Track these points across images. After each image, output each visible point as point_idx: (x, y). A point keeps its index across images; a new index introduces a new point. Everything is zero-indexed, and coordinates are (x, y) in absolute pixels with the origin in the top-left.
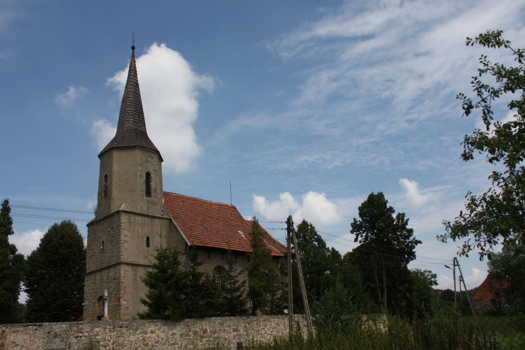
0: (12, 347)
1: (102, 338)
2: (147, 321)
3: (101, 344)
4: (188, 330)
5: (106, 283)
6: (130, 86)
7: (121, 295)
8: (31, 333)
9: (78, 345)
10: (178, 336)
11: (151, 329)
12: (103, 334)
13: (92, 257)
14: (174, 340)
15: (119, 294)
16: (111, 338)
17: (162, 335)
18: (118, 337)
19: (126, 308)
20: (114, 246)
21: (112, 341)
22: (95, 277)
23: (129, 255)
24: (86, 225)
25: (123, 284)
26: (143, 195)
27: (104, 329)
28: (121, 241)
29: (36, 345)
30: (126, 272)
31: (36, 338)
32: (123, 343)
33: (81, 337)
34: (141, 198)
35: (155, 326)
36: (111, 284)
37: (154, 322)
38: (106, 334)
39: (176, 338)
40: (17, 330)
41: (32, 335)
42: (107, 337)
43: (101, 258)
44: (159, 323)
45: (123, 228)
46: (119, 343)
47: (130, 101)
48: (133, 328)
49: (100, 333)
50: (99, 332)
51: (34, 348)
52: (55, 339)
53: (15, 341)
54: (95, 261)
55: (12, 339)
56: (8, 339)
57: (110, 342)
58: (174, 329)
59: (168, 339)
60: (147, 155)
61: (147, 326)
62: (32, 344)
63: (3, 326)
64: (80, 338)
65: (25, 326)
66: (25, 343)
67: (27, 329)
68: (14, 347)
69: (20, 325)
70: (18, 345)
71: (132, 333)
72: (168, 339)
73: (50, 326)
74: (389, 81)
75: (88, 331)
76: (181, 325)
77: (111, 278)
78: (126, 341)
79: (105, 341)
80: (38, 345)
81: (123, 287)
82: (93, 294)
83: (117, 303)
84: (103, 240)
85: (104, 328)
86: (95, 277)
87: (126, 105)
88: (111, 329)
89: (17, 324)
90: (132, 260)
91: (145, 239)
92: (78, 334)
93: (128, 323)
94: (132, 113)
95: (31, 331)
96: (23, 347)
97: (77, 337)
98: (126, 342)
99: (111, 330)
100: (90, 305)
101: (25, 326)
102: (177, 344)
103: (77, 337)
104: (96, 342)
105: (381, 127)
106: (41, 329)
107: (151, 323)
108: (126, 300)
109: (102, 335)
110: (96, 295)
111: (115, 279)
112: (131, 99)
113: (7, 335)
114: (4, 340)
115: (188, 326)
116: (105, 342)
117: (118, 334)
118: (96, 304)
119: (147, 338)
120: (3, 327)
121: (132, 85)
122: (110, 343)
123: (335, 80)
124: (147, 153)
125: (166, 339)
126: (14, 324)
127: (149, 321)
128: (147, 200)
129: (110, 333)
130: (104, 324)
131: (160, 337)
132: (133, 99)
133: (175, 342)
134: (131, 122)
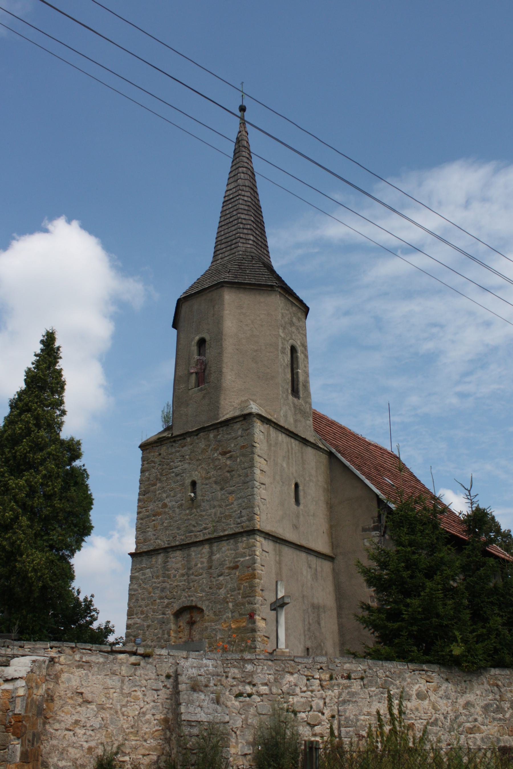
0: (74, 707)
1: (304, 703)
2: (406, 667)
3: (303, 719)
4: (498, 697)
5: (204, 575)
6: (242, 175)
7: (257, 605)
8: (123, 673)
9: (243, 716)
10: (478, 709)
11: (417, 687)
12: (304, 692)
13: (154, 516)
14: (471, 719)
15: (250, 603)
16: (325, 703)
17: (444, 706)
18: (344, 702)
19: (266, 639)
20: (231, 493)
21: (327, 712)
22: (165, 562)
23: (269, 515)
24: (139, 443)
25: (261, 579)
26: (287, 390)
27: (308, 680)
28: (255, 480)
29: (137, 707)
30: (264, 553)
31: (136, 689)
32: (358, 720)
33: (250, 695)
34: (284, 396)
35: (427, 682)
36: (221, 578)
37: (423, 670)
38: (312, 691)
39: (476, 716)
40: (87, 662)
41: (127, 679)
42: (316, 700)
43: (188, 519)
44: (434, 675)
45: (259, 454)
46: (346, 718)
47: (244, 203)
48: (377, 682)
49: (298, 690)
50: (296, 685)
51: (131, 714)
52: (195, 695)
53: (83, 691)
54: (165, 524)
55: (75, 683)
56: (62, 682)
57: (323, 714)
58: (468, 691)
59: (456, 717)
60: (291, 310)
61: (409, 680)
62: (128, 701)
63: (49, 645)
64: (248, 699)
65: (108, 652)
66: (108, 698)
67: (112, 661)
68: (80, 705)
69: (94, 647)
70: (89, 702)
71: (375, 695)
72: (456, 717)
73: (171, 660)
74: (435, 325)
75: (269, 680)
76: (483, 684)
77: (222, 564)
78: (364, 715)
79: (310, 710)
80: (141, 708)
81: (260, 588)
82: (158, 601)
83: (244, 624)
84: (195, 478)
85: (306, 676)
86: (165, 562)
87: (237, 209)
88: (326, 681)
89: (89, 646)
90: (273, 529)
91: (293, 486)
92: (244, 686)
93: (365, 668)
94: (250, 225)
95: (123, 668)
96: (103, 709)
97: (239, 695)
98: (362, 717)
99: (324, 683)
100: (148, 626)
101: (108, 652)
102: (479, 731)
103: (239, 695)
104: (287, 711)
105: (414, 399)
106: (148, 666)
107: (417, 672)
108: (265, 619)
109: (303, 694)
110: (168, 604)
111: (236, 567)
112: (246, 198)
113: (62, 671)
114: (53, 684)
115: (498, 686)
116: (311, 713)
117: (344, 695)
118: (168, 623)
119: (411, 710)
120: (51, 648)
121: (246, 174)
122: (324, 718)
123: (347, 313)
124: (290, 306)
125: (453, 717)
126: (79, 645)
127: (411, 666)
128: (294, 404)
129: (322, 692)
130: (308, 666)
131: (439, 710)
132: (250, 200)
133: (475, 726)
134: (251, 242)
